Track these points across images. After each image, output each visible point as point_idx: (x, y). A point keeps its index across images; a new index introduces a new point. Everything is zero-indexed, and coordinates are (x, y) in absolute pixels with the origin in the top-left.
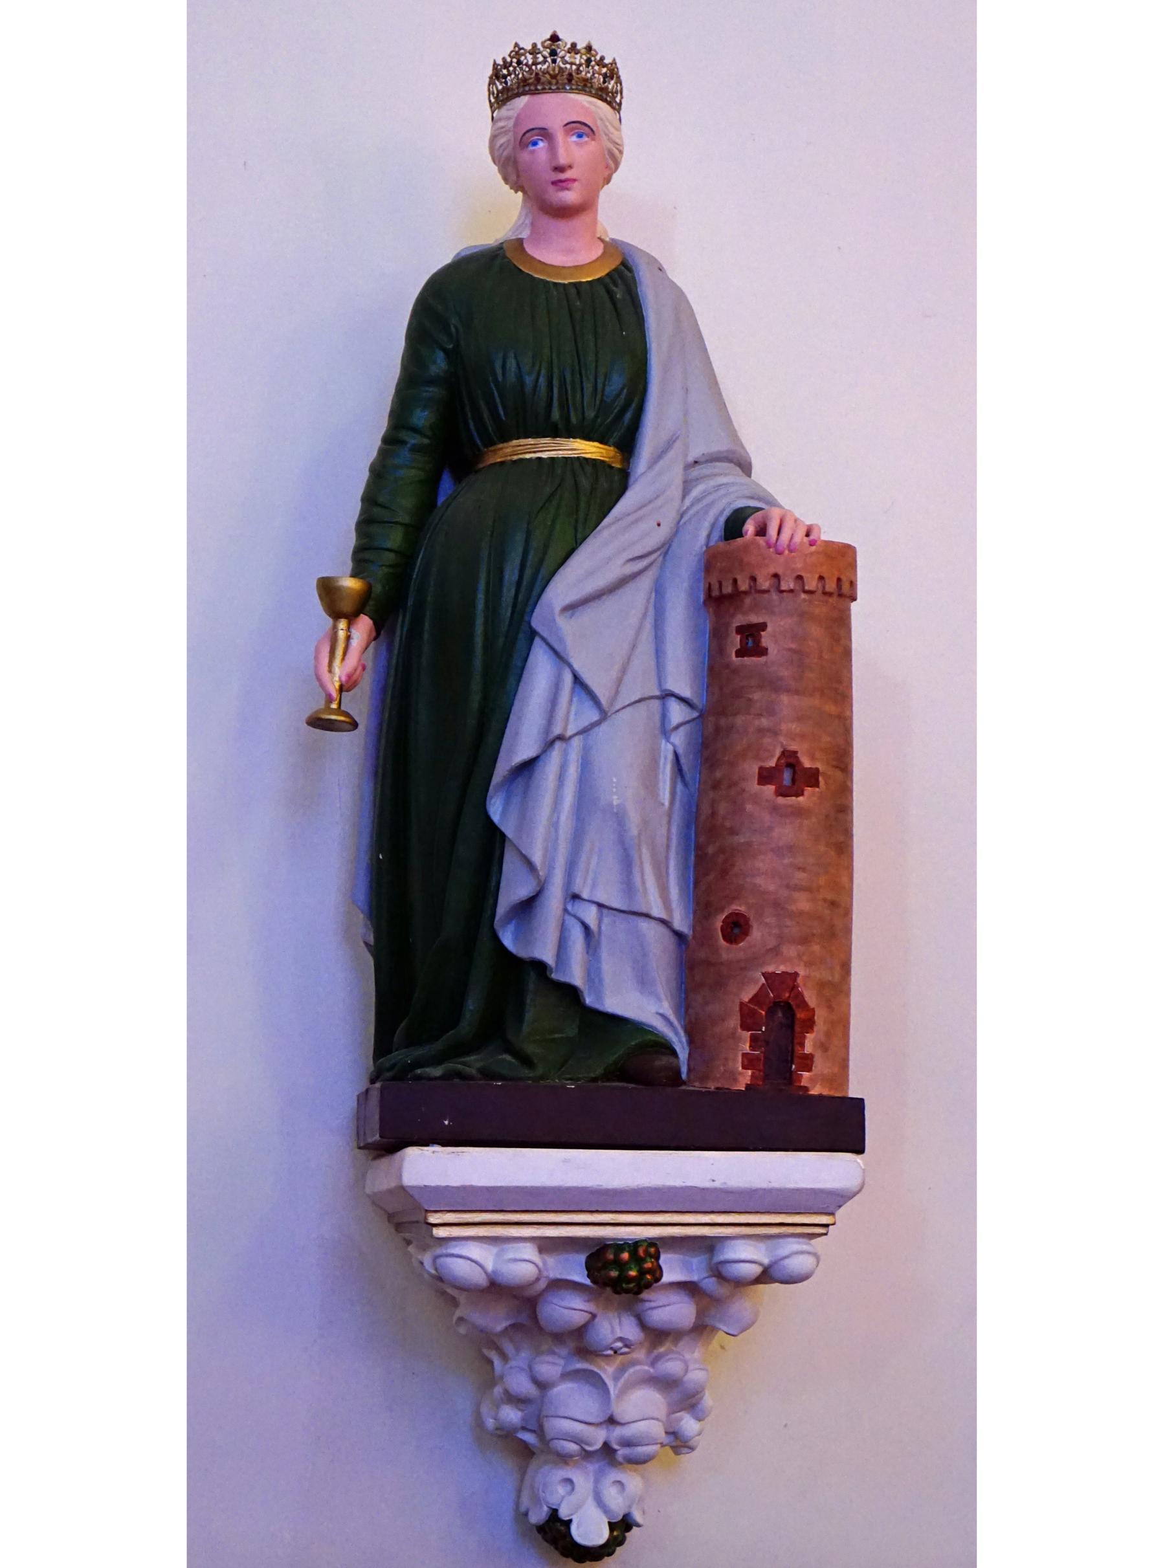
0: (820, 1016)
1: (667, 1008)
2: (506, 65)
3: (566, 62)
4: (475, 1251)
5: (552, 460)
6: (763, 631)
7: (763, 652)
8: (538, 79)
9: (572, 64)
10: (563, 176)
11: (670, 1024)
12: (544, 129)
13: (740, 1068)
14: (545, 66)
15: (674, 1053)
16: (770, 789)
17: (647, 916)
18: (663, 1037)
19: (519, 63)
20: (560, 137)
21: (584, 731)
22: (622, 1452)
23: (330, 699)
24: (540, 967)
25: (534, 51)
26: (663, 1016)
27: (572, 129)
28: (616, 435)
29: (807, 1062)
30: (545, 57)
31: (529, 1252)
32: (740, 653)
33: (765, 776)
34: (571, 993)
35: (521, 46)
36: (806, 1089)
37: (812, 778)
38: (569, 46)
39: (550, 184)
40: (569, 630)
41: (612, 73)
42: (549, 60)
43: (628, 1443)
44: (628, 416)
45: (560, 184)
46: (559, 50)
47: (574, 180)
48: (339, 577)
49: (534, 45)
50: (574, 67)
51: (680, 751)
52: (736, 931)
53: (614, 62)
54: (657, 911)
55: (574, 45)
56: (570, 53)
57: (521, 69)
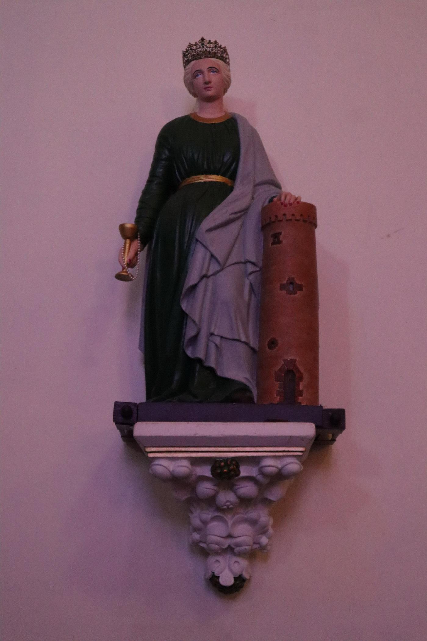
0: (305, 376)
1: (248, 376)
2: (187, 51)
3: (207, 47)
4: (164, 463)
5: (205, 182)
6: (281, 235)
7: (280, 242)
8: (198, 54)
9: (210, 47)
10: (207, 86)
11: (250, 382)
12: (201, 70)
13: (275, 396)
14: (200, 49)
15: (249, 390)
16: (284, 292)
17: (239, 341)
18: (246, 385)
19: (191, 49)
20: (206, 73)
21: (214, 274)
22: (237, 549)
23: (123, 268)
24: (199, 360)
25: (196, 44)
26: (246, 378)
27: (210, 70)
28: (229, 174)
29: (301, 393)
30: (200, 46)
31: (186, 463)
32: (273, 244)
33: (282, 287)
34: (211, 370)
35: (192, 43)
36: (300, 403)
37: (300, 288)
38: (208, 41)
39: (204, 90)
40: (208, 238)
41: (225, 51)
42: (201, 47)
43: (238, 545)
44: (233, 167)
45: (207, 89)
46: (205, 43)
47: (211, 87)
48: (126, 224)
49: (196, 42)
50: (211, 48)
51: (252, 282)
52: (273, 345)
53: (225, 47)
54: (243, 339)
55: (210, 41)
56: (209, 44)
57: (192, 51)
